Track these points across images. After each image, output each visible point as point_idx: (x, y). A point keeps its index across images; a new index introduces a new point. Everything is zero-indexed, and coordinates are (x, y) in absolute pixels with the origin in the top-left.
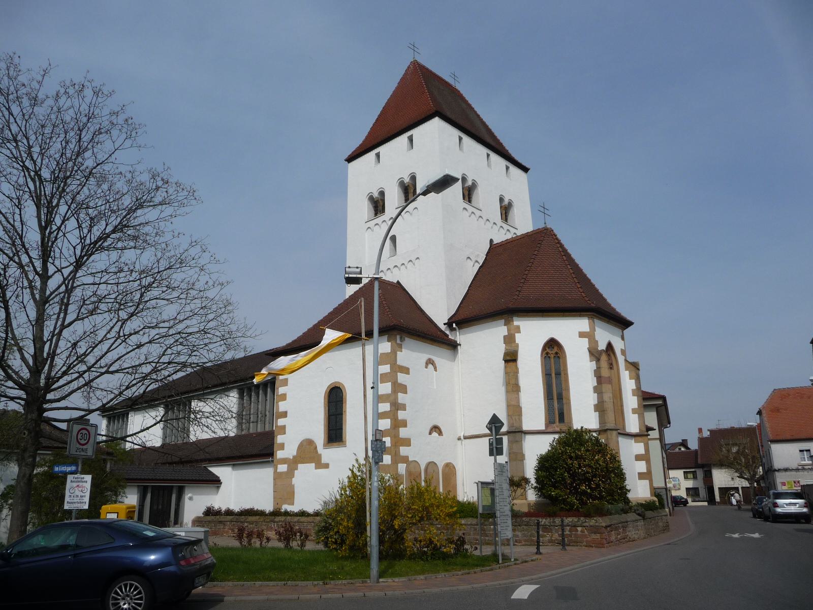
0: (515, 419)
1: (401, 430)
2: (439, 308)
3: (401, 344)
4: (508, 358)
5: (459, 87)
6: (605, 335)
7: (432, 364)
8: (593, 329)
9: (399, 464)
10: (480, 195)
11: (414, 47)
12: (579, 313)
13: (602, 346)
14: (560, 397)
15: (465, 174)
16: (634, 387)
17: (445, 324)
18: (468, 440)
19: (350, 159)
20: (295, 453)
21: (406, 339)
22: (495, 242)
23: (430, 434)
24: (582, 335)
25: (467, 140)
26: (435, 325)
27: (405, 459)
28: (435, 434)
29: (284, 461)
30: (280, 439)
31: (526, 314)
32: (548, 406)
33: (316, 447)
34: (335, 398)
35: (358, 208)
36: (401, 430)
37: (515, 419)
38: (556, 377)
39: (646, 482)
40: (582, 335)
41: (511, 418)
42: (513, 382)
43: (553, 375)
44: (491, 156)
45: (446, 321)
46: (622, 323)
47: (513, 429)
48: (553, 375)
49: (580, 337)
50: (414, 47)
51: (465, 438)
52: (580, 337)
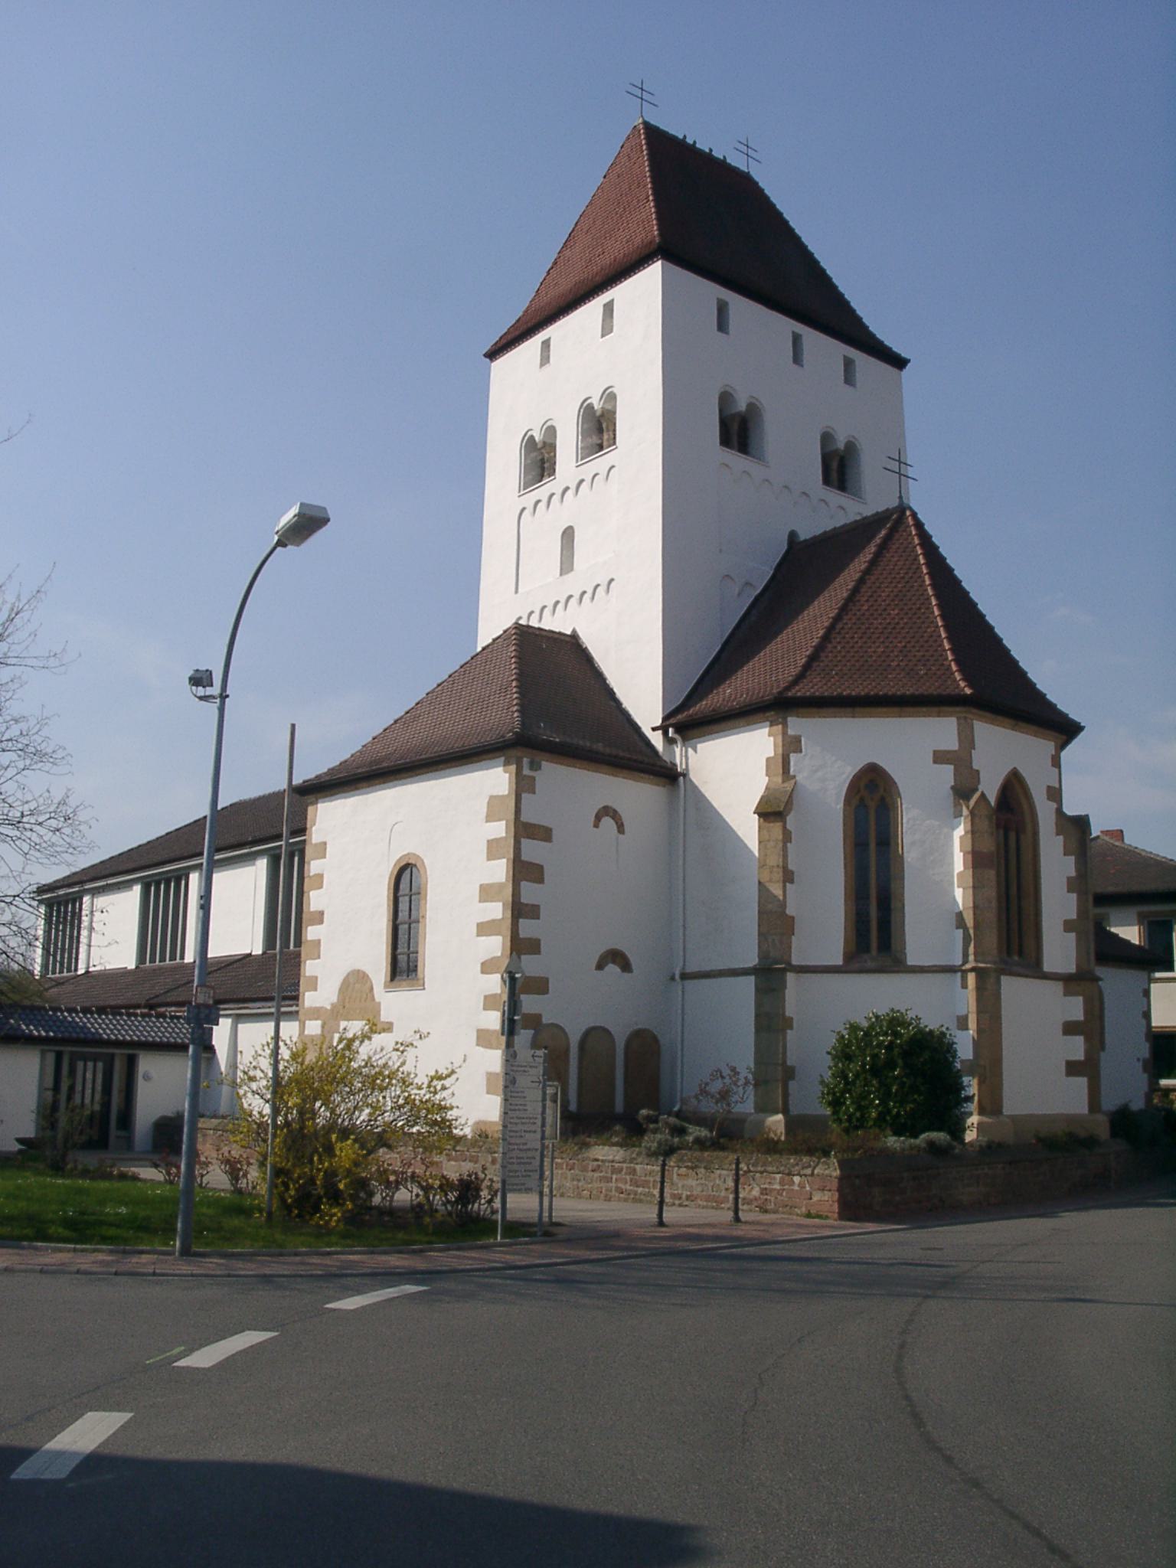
1: (1079, 1055)
2: (642, 692)
5: (756, 175)
6: (1001, 750)
8: (967, 741)
10: (773, 433)
11: (641, 93)
13: (990, 787)
16: (1073, 874)
18: (687, 983)
19: (494, 354)
20: (334, 999)
23: (600, 966)
24: (940, 757)
25: (741, 307)
26: (637, 729)
28: (612, 969)
29: (316, 1013)
30: (310, 968)
33: (372, 989)
34: (406, 883)
35: (503, 462)
36: (1079, 1055)
39: (1082, 1082)
40: (940, 757)
43: (872, 846)
44: (804, 338)
46: (1065, 729)
48: (872, 846)
49: (935, 762)
50: (641, 93)
51: (685, 976)
52: (935, 762)
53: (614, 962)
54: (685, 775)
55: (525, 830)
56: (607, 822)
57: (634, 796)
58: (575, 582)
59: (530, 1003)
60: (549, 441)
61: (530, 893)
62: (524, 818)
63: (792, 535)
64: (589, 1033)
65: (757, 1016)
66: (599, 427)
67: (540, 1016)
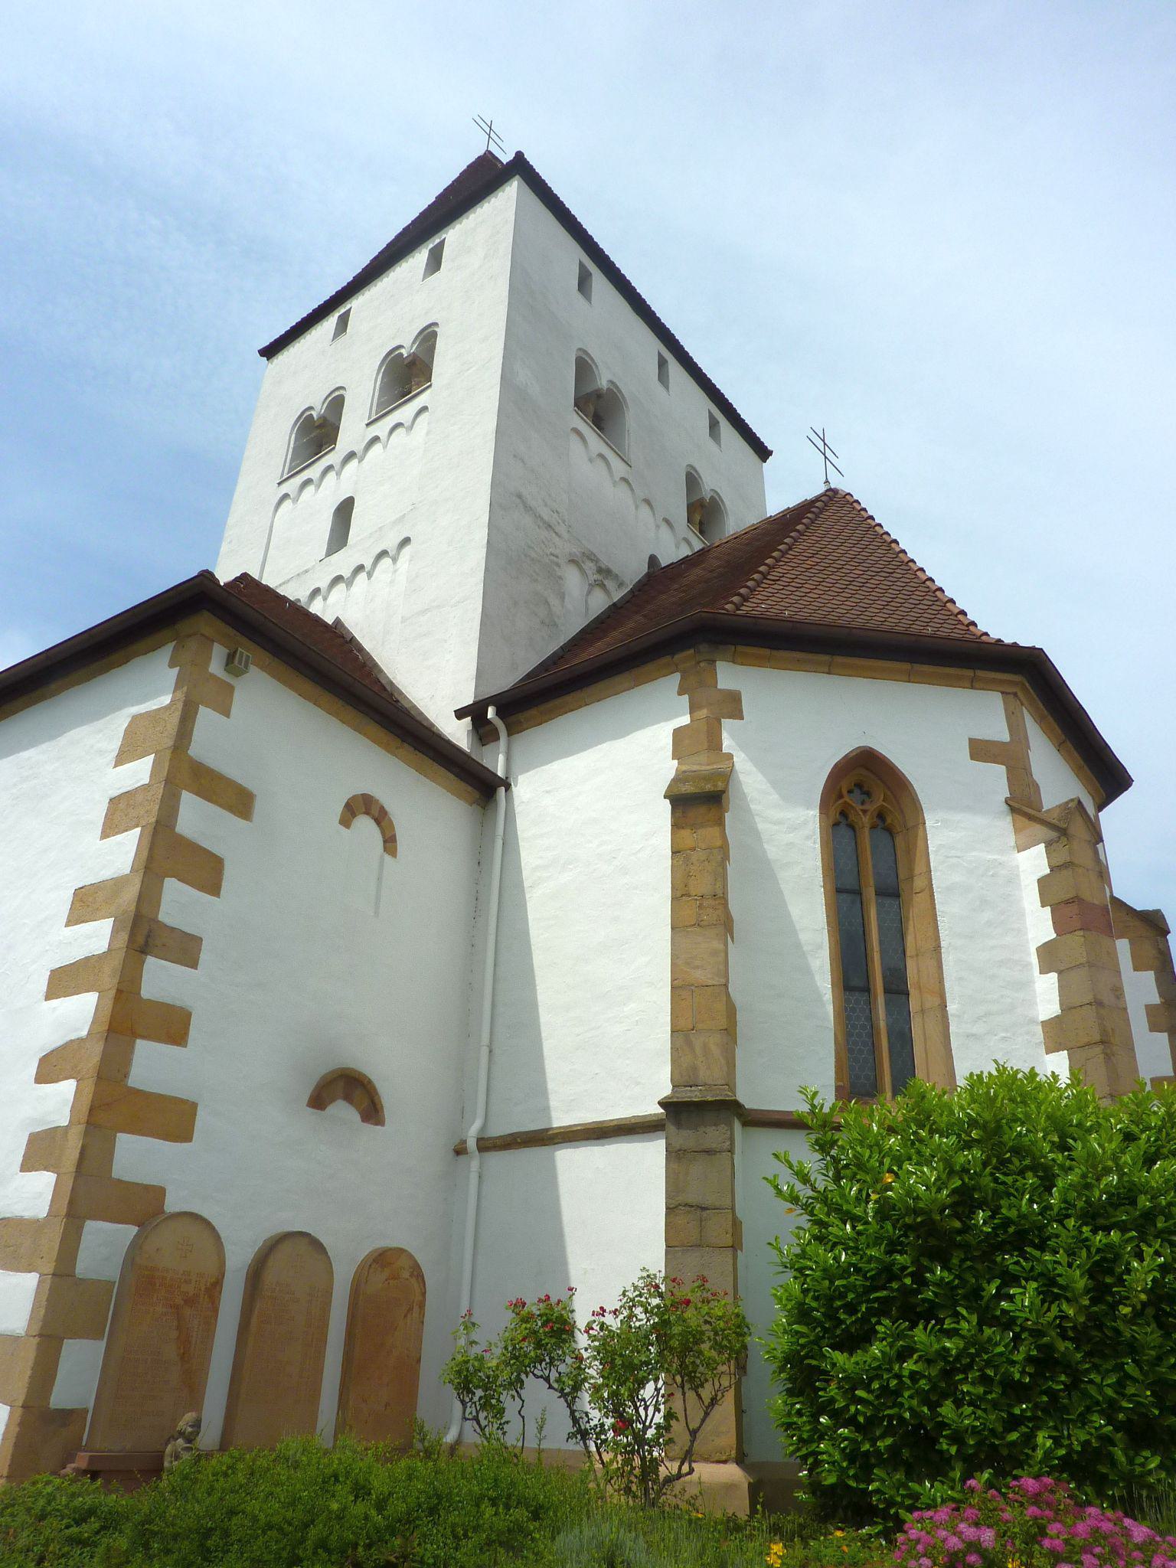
0: (705, 1046)
3: (230, 689)
4: (688, 788)
7: (378, 822)
9: (91, 1226)
12: (970, 673)
14: (897, 988)
15: (585, 352)
16: (1155, 999)
17: (460, 714)
18: (496, 1159)
21: (253, 669)
22: (664, 562)
27: (143, 1206)
28: (343, 1111)
31: (766, 652)
32: (848, 1018)
37: (705, 1046)
38: (880, 906)
40: (981, 750)
41: (689, 1044)
42: (702, 885)
45: (468, 700)
47: (695, 1095)
48: (870, 893)
51: (486, 1145)
53: (348, 1098)
54: (508, 787)
55: (185, 773)
56: (365, 825)
57: (425, 807)
58: (343, 562)
59: (136, 1156)
60: (331, 418)
61: (179, 904)
62: (196, 750)
63: (653, 560)
64: (383, 1259)
65: (670, 1210)
66: (407, 374)
67: (160, 1192)
